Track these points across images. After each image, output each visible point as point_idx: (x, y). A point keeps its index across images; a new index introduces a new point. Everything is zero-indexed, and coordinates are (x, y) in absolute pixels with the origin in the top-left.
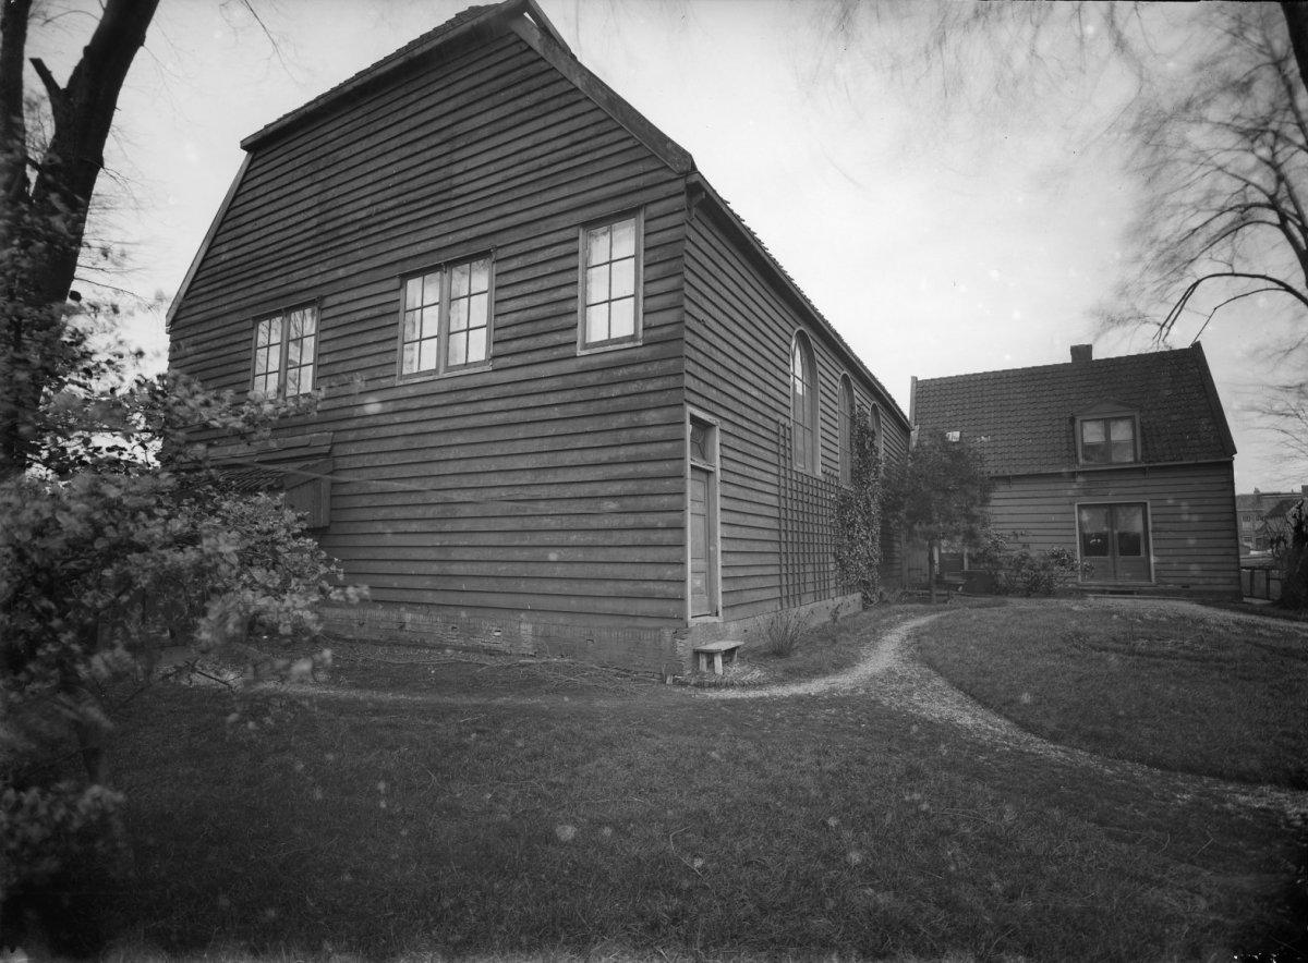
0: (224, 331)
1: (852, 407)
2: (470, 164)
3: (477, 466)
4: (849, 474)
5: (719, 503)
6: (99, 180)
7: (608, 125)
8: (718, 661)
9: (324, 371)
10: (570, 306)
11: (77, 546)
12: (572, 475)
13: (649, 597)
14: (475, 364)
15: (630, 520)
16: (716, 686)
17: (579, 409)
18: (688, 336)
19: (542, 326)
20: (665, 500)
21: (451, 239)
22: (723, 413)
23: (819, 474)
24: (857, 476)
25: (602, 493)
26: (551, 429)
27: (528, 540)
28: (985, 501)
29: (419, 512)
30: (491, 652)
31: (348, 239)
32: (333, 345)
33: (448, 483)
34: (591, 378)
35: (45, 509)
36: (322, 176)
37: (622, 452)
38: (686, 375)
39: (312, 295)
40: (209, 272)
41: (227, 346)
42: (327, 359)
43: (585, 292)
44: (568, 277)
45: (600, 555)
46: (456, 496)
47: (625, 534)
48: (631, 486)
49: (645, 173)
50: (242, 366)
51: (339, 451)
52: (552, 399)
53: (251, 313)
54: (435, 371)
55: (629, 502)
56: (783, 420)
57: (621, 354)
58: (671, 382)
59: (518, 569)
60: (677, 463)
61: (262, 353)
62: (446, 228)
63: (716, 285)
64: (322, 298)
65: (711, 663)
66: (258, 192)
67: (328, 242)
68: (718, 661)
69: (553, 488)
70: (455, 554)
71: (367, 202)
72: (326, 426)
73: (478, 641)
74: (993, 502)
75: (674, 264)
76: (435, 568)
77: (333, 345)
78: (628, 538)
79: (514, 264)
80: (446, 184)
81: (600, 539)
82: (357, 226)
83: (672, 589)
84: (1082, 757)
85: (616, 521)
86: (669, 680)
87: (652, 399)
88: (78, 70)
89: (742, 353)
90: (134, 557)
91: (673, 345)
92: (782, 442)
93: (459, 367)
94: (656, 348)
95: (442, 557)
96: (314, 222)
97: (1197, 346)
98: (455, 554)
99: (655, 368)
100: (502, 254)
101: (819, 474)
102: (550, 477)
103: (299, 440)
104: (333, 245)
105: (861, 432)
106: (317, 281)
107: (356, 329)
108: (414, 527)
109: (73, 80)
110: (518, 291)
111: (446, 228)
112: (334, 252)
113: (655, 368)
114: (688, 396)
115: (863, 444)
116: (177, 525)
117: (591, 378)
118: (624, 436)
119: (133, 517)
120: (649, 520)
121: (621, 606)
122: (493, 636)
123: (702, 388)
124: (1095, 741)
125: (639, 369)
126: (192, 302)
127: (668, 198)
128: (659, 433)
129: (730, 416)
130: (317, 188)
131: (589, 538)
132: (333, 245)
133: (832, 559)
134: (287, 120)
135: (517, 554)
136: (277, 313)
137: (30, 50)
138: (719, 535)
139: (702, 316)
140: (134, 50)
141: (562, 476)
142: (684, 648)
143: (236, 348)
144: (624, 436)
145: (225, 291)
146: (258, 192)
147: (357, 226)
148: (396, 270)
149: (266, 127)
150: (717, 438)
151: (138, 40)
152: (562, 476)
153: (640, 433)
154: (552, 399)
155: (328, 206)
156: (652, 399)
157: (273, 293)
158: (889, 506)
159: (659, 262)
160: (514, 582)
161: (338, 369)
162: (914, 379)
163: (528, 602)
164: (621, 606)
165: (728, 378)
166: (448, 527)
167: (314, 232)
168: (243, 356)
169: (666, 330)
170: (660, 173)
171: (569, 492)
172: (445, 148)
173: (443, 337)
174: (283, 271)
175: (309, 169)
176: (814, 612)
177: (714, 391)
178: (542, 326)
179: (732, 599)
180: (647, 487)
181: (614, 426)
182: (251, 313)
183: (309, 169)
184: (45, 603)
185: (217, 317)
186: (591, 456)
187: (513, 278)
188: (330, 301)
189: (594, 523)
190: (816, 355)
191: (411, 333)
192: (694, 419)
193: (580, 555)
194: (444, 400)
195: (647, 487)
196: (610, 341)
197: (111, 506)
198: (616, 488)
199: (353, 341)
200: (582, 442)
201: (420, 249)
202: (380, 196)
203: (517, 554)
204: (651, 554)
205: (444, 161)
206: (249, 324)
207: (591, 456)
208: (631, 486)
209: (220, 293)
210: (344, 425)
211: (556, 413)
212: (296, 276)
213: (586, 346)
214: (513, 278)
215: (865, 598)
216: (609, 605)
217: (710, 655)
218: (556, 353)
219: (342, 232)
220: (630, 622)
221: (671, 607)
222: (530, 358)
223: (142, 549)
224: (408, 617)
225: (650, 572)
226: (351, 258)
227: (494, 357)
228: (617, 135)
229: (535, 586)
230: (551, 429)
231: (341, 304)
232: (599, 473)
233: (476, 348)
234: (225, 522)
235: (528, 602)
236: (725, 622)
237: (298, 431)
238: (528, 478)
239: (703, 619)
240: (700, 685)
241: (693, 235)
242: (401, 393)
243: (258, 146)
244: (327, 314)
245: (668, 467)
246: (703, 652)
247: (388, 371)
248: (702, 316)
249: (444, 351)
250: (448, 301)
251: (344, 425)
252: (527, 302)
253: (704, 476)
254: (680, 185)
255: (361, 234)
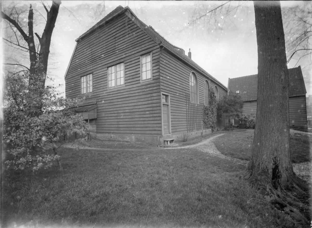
0: (75, 79)
1: (209, 87)
2: (119, 43)
3: (123, 105)
4: (208, 103)
5: (170, 111)
6: (49, 54)
7: (145, 34)
8: (169, 142)
9: (94, 87)
10: (139, 72)
11: (51, 123)
12: (141, 107)
13: (155, 130)
14: (122, 85)
15: (151, 115)
16: (167, 147)
17: (141, 94)
18: (161, 78)
19: (134, 77)
20: (157, 111)
21: (116, 59)
22: (171, 92)
23: (199, 103)
24: (210, 103)
25: (146, 110)
26: (136, 98)
27: (133, 120)
28: (242, 107)
29: (113, 115)
30: (127, 142)
31: (97, 60)
32: (96, 82)
33: (118, 109)
34: (143, 87)
35: (47, 119)
36: (91, 47)
37: (149, 102)
38: (161, 86)
39: (91, 72)
40: (71, 67)
41: (102, 47)
42: (95, 85)
43: (142, 70)
44: (138, 66)
45: (146, 122)
46: (120, 112)
47: (150, 118)
48: (151, 109)
49: (152, 44)
50: (79, 87)
51: (98, 103)
52: (136, 91)
53: (80, 76)
54: (115, 87)
55: (151, 112)
56: (187, 92)
57: (149, 82)
58: (158, 87)
59: (131, 126)
60: (159, 104)
61: (82, 84)
62: (115, 57)
63: (168, 66)
64: (93, 72)
65: (167, 143)
66: (79, 50)
67: (93, 60)
68: (169, 142)
69: (137, 109)
70: (120, 123)
71: (100, 52)
72: (95, 98)
73: (125, 140)
74: (244, 107)
75: (158, 63)
76: (117, 126)
77: (96, 82)
78: (151, 119)
79: (128, 64)
80: (114, 48)
81: (146, 119)
82: (98, 57)
83: (159, 129)
84: (229, 158)
85: (148, 116)
86: (159, 146)
87: (155, 91)
88: (43, 34)
89: (176, 79)
90: (58, 124)
91: (158, 80)
92: (187, 97)
93: (119, 86)
94: (155, 80)
95: (118, 124)
96: (90, 56)
97: (300, 67)
98: (120, 123)
99: (155, 85)
100: (126, 62)
101: (199, 103)
102: (136, 107)
103: (91, 101)
104: (94, 61)
105: (211, 93)
106: (92, 69)
107: (100, 78)
108: (112, 118)
109: (43, 36)
110: (129, 69)
111: (115, 57)
112: (94, 63)
113: (155, 85)
114: (161, 90)
115: (211, 95)
116: (64, 120)
117: (143, 87)
118: (150, 99)
119: (58, 119)
120: (155, 115)
121: (150, 132)
122: (128, 139)
123: (165, 88)
124: (232, 155)
125: (152, 85)
126: (69, 74)
127: (157, 49)
128: (156, 98)
129: (173, 93)
130: (90, 49)
131: (144, 119)
132: (94, 61)
133: (202, 122)
134: (84, 35)
135: (131, 123)
136: (85, 76)
137: (34, 31)
138: (170, 117)
139: (165, 73)
140: (53, 28)
141: (139, 107)
142: (162, 140)
143: (77, 83)
144: (150, 99)
145: (75, 71)
146: (79, 50)
147: (98, 57)
148: (106, 66)
149: (80, 37)
150: (169, 98)
151: (54, 26)
152: (139, 107)
153: (153, 98)
154: (136, 91)
155: (93, 53)
156: (155, 91)
157: (84, 71)
158: (219, 109)
159: (156, 63)
160: (131, 128)
161: (97, 86)
162: (229, 79)
163: (134, 132)
164: (150, 132)
165: (172, 85)
166: (118, 118)
167: (90, 59)
168: (79, 85)
169: (157, 77)
170: (155, 44)
171: (140, 110)
172: (114, 40)
173: (116, 80)
174: (85, 67)
175: (89, 45)
176: (194, 134)
177: (169, 88)
178: (134, 77)
179: (174, 130)
180: (154, 109)
181: (148, 97)
182: (80, 76)
183: (89, 45)
184: (48, 131)
185: (74, 77)
186: (144, 103)
187: (128, 67)
188: (94, 73)
189: (145, 116)
190: (197, 77)
191: (109, 78)
192: (163, 94)
193: (142, 122)
194: (116, 92)
195: (154, 109)
196: (147, 79)
197: (55, 118)
198: (149, 109)
199: (99, 81)
200: (142, 100)
201: (110, 61)
202: (102, 51)
203: (131, 123)
204: (155, 122)
205: (114, 43)
206: (80, 78)
207: (144, 103)
208: (151, 109)
209: (74, 72)
210: (99, 98)
211: (137, 94)
212: (88, 68)
213: (142, 81)
214: (128, 67)
215: (212, 130)
216: (148, 132)
217: (167, 141)
218: (137, 82)
219: (96, 58)
220: (152, 135)
221: (159, 132)
222: (132, 83)
223: (59, 123)
224: (112, 135)
225: (155, 125)
226: (98, 64)
227: (125, 83)
228: (146, 36)
229: (135, 129)
230: (136, 98)
231: (96, 73)
232: (145, 106)
233: (122, 82)
234: (71, 119)
235: (134, 132)
236: (172, 135)
237: (90, 99)
238: (132, 108)
239: (167, 135)
240: (165, 147)
241: (162, 56)
242: (108, 91)
243: (79, 41)
244: (94, 75)
245: (158, 104)
246: (166, 141)
247: (106, 87)
248: (165, 73)
249: (116, 82)
250: (116, 72)
251: (99, 98)
252: (131, 72)
253: (167, 106)
254: (158, 46)
255: (99, 59)
